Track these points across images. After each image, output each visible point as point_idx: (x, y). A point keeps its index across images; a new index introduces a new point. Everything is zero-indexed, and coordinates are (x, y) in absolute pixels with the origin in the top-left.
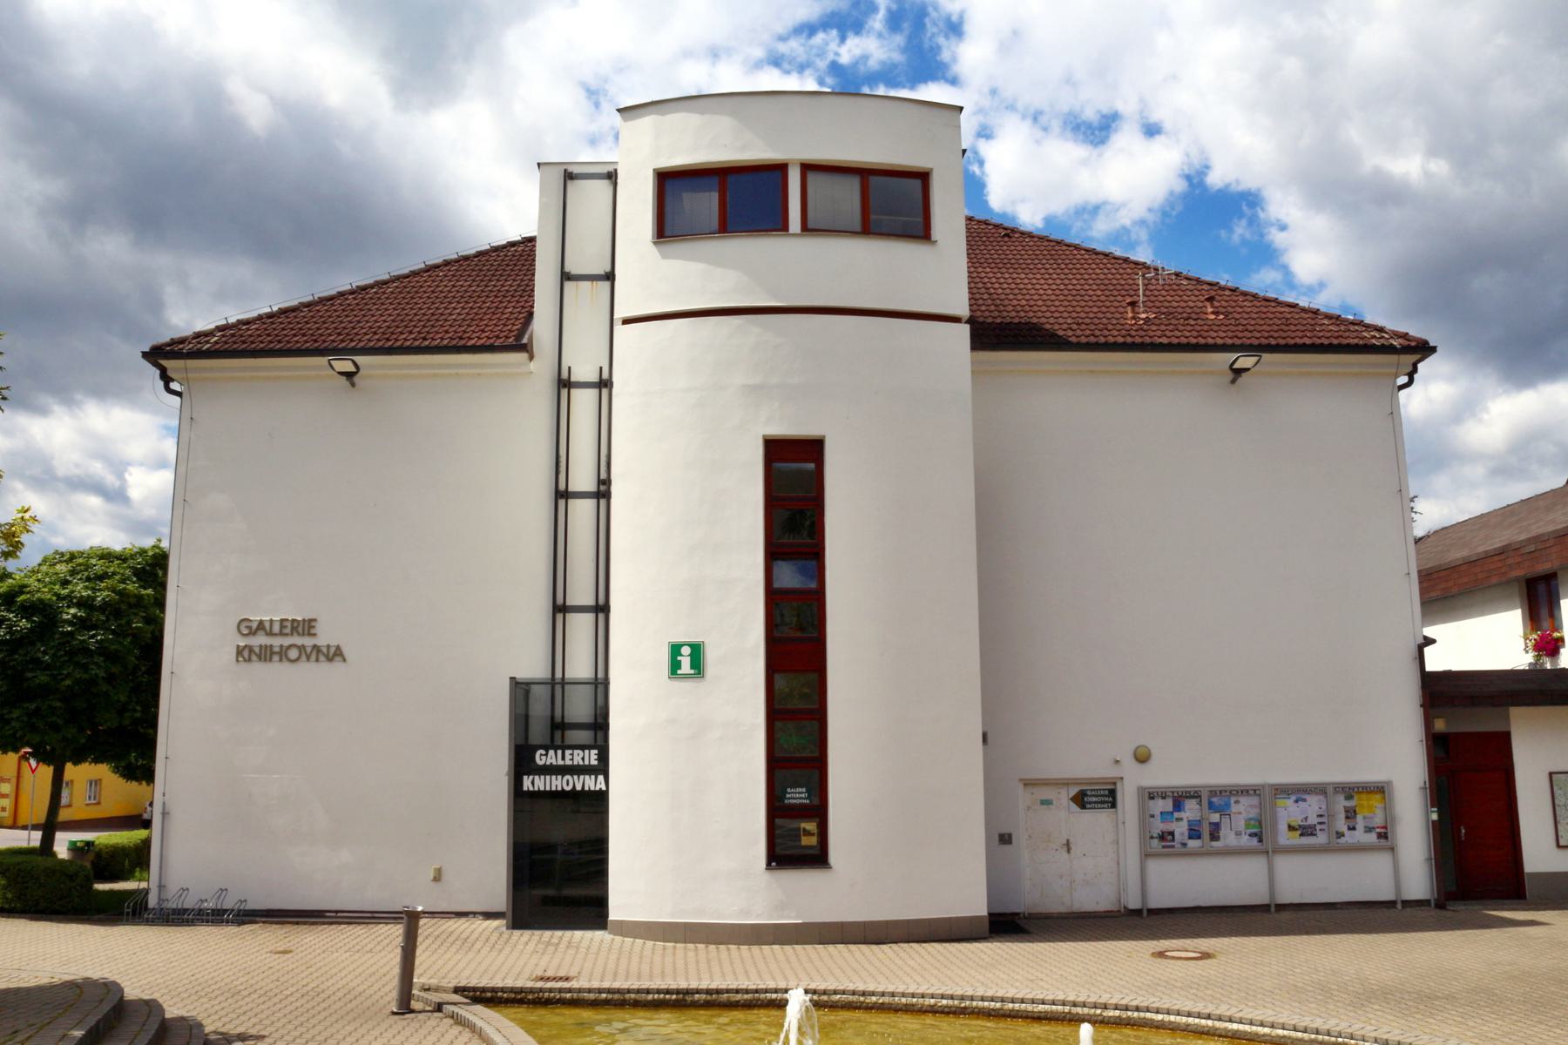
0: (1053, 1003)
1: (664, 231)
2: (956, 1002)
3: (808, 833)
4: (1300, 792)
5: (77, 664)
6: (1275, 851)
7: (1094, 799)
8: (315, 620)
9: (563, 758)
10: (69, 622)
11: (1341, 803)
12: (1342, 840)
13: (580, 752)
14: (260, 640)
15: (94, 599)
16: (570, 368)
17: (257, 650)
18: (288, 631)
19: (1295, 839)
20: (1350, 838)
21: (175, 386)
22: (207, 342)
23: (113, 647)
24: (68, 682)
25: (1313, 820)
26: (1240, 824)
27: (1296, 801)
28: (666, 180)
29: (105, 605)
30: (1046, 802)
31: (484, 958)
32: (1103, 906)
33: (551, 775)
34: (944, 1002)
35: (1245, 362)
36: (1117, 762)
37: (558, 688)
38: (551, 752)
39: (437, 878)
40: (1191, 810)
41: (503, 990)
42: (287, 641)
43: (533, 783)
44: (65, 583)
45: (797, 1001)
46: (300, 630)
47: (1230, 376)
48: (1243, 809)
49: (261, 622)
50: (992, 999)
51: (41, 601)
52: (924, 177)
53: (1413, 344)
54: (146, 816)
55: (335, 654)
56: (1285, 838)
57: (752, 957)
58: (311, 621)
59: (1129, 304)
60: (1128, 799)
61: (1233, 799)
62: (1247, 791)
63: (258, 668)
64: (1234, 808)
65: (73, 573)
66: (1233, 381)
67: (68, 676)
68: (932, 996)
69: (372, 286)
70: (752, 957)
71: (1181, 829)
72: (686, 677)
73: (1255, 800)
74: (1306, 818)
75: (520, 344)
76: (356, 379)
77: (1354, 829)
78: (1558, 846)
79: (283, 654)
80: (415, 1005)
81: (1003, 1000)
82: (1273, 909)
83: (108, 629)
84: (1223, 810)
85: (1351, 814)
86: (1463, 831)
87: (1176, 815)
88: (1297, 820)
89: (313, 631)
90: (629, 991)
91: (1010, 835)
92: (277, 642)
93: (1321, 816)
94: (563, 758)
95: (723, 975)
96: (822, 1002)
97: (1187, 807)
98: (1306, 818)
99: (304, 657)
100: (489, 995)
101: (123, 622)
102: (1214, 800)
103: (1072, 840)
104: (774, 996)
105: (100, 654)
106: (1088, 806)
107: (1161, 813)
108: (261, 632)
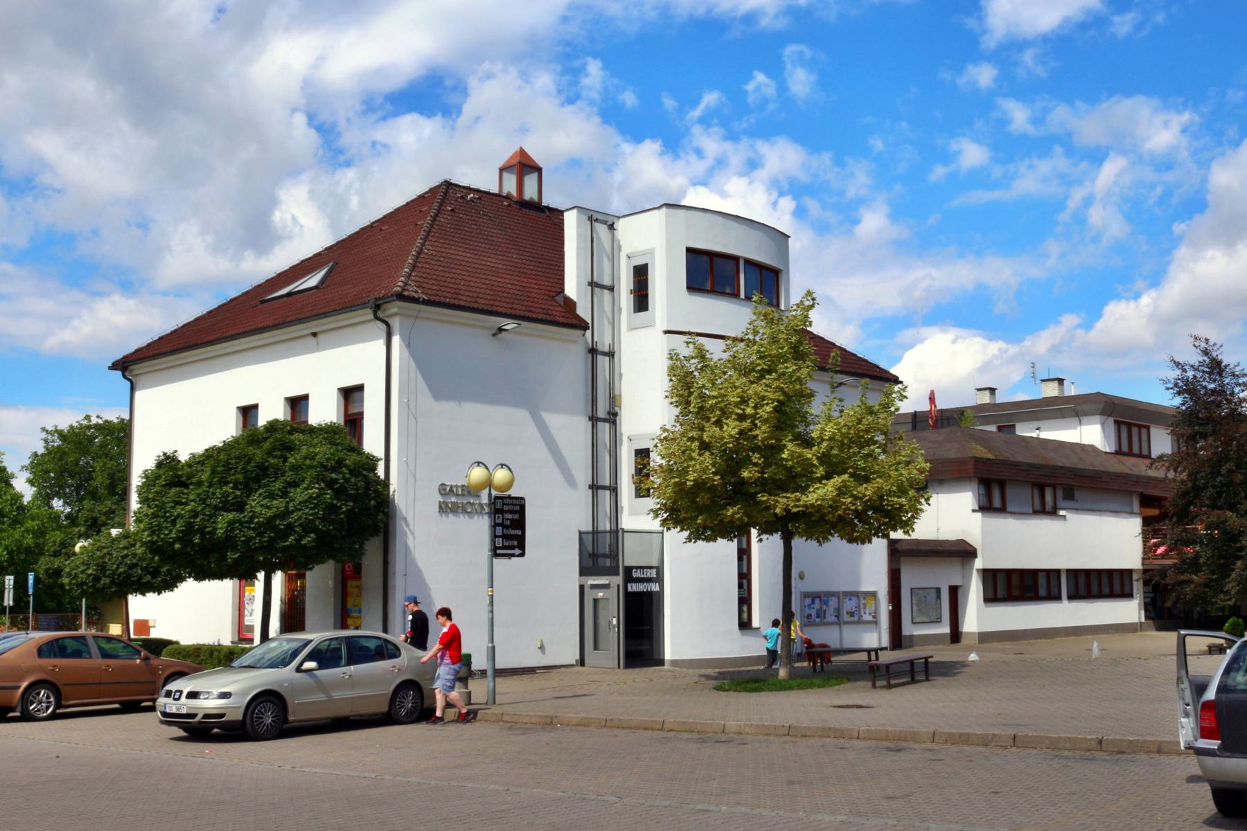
54: (350, 621)
56: (846, 618)
78: (913, 623)
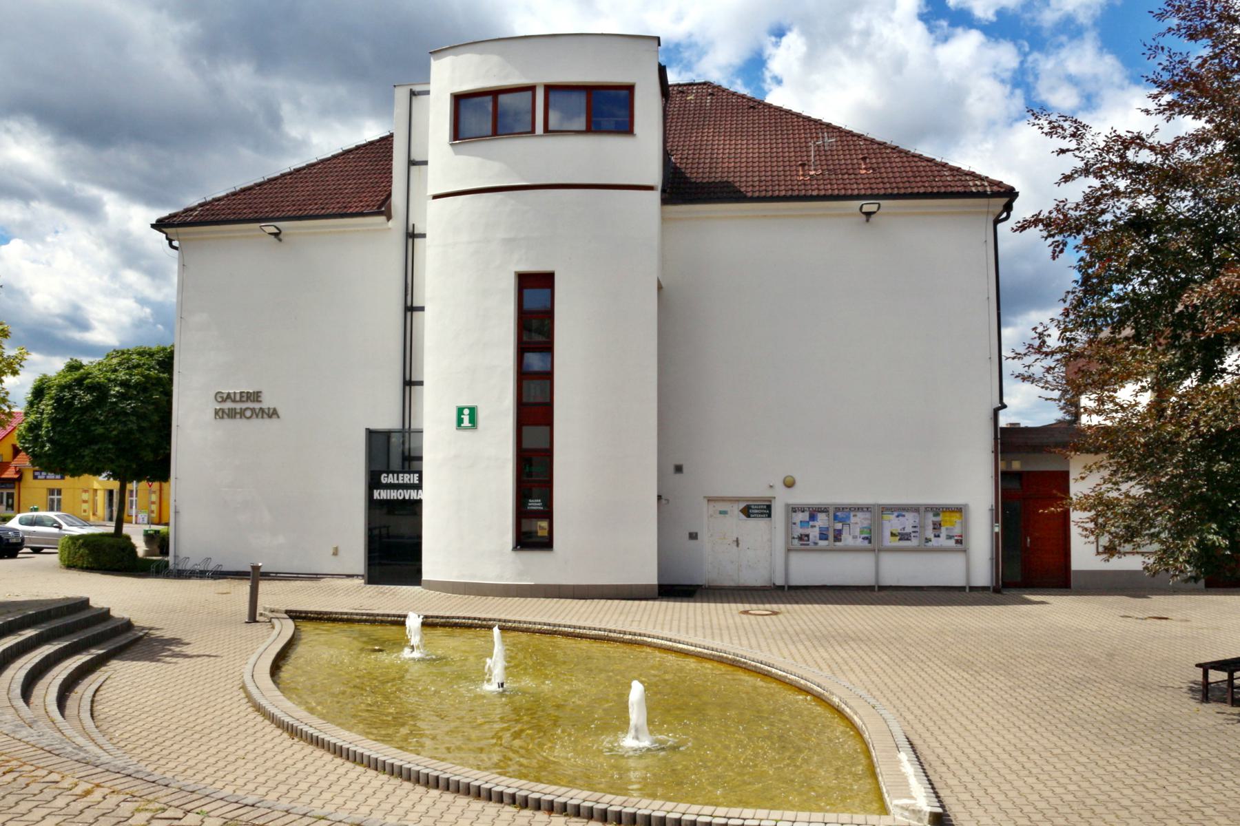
0: (600, 630)
1: (457, 134)
2: (551, 628)
3: (542, 528)
4: (901, 510)
5: (120, 422)
6: (880, 550)
7: (756, 511)
8: (260, 392)
9: (398, 479)
10: (114, 396)
11: (931, 518)
12: (930, 544)
13: (408, 475)
14: (228, 405)
15: (130, 380)
16: (414, 225)
17: (227, 411)
18: (244, 399)
19: (896, 542)
20: (935, 542)
21: (175, 243)
22: (191, 215)
23: (142, 411)
24: (115, 433)
25: (909, 530)
26: (857, 532)
27: (898, 516)
28: (459, 100)
29: (137, 384)
30: (724, 513)
31: (664, 620)
32: (759, 582)
33: (390, 489)
34: (545, 627)
35: (870, 207)
36: (771, 486)
37: (407, 435)
38: (391, 475)
39: (336, 553)
40: (822, 521)
41: (311, 612)
42: (244, 406)
43: (380, 494)
44: (115, 371)
45: (414, 622)
46: (252, 398)
47: (864, 217)
48: (859, 521)
49: (229, 394)
50: (569, 627)
51: (98, 383)
52: (630, 89)
53: (1002, 190)
55: (273, 414)
56: (889, 542)
57: (780, 621)
58: (258, 392)
59: (801, 165)
60: (778, 511)
61: (852, 514)
62: (862, 509)
63: (227, 422)
64: (853, 520)
65: (120, 364)
66: (868, 221)
67: (114, 429)
68: (540, 624)
69: (303, 168)
70: (780, 621)
71: (814, 533)
72: (466, 428)
73: (868, 515)
74: (904, 529)
75: (383, 208)
76: (281, 236)
77: (939, 536)
79: (242, 413)
80: (258, 618)
81: (575, 627)
82: (876, 589)
83: (139, 399)
84: (844, 521)
85: (937, 526)
86: (1029, 540)
87: (811, 523)
88: (897, 530)
89: (259, 399)
90: (378, 615)
91: (696, 534)
92: (238, 406)
93: (915, 527)
94: (398, 479)
95: (679, 631)
96: (429, 624)
97: (819, 519)
98: (904, 529)
99: (254, 416)
100: (304, 615)
101: (148, 395)
102: (839, 514)
103: (740, 538)
104: (457, 621)
105: (133, 415)
106: (752, 516)
107: (801, 522)
108: (229, 400)
